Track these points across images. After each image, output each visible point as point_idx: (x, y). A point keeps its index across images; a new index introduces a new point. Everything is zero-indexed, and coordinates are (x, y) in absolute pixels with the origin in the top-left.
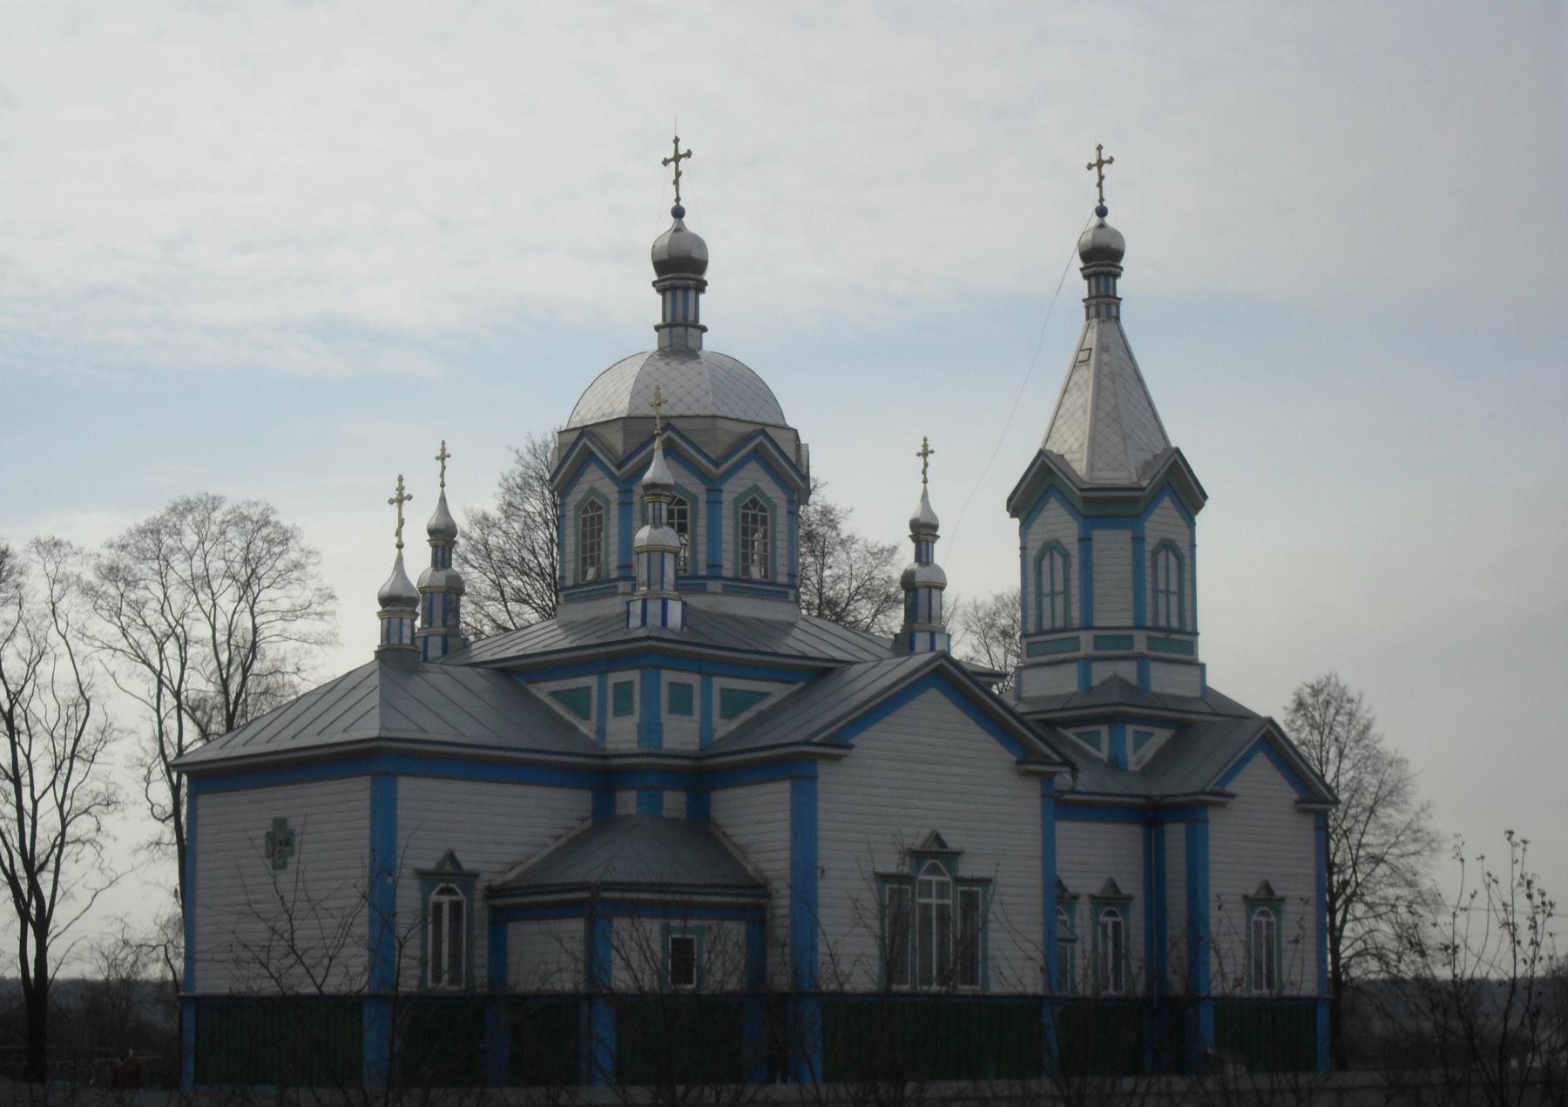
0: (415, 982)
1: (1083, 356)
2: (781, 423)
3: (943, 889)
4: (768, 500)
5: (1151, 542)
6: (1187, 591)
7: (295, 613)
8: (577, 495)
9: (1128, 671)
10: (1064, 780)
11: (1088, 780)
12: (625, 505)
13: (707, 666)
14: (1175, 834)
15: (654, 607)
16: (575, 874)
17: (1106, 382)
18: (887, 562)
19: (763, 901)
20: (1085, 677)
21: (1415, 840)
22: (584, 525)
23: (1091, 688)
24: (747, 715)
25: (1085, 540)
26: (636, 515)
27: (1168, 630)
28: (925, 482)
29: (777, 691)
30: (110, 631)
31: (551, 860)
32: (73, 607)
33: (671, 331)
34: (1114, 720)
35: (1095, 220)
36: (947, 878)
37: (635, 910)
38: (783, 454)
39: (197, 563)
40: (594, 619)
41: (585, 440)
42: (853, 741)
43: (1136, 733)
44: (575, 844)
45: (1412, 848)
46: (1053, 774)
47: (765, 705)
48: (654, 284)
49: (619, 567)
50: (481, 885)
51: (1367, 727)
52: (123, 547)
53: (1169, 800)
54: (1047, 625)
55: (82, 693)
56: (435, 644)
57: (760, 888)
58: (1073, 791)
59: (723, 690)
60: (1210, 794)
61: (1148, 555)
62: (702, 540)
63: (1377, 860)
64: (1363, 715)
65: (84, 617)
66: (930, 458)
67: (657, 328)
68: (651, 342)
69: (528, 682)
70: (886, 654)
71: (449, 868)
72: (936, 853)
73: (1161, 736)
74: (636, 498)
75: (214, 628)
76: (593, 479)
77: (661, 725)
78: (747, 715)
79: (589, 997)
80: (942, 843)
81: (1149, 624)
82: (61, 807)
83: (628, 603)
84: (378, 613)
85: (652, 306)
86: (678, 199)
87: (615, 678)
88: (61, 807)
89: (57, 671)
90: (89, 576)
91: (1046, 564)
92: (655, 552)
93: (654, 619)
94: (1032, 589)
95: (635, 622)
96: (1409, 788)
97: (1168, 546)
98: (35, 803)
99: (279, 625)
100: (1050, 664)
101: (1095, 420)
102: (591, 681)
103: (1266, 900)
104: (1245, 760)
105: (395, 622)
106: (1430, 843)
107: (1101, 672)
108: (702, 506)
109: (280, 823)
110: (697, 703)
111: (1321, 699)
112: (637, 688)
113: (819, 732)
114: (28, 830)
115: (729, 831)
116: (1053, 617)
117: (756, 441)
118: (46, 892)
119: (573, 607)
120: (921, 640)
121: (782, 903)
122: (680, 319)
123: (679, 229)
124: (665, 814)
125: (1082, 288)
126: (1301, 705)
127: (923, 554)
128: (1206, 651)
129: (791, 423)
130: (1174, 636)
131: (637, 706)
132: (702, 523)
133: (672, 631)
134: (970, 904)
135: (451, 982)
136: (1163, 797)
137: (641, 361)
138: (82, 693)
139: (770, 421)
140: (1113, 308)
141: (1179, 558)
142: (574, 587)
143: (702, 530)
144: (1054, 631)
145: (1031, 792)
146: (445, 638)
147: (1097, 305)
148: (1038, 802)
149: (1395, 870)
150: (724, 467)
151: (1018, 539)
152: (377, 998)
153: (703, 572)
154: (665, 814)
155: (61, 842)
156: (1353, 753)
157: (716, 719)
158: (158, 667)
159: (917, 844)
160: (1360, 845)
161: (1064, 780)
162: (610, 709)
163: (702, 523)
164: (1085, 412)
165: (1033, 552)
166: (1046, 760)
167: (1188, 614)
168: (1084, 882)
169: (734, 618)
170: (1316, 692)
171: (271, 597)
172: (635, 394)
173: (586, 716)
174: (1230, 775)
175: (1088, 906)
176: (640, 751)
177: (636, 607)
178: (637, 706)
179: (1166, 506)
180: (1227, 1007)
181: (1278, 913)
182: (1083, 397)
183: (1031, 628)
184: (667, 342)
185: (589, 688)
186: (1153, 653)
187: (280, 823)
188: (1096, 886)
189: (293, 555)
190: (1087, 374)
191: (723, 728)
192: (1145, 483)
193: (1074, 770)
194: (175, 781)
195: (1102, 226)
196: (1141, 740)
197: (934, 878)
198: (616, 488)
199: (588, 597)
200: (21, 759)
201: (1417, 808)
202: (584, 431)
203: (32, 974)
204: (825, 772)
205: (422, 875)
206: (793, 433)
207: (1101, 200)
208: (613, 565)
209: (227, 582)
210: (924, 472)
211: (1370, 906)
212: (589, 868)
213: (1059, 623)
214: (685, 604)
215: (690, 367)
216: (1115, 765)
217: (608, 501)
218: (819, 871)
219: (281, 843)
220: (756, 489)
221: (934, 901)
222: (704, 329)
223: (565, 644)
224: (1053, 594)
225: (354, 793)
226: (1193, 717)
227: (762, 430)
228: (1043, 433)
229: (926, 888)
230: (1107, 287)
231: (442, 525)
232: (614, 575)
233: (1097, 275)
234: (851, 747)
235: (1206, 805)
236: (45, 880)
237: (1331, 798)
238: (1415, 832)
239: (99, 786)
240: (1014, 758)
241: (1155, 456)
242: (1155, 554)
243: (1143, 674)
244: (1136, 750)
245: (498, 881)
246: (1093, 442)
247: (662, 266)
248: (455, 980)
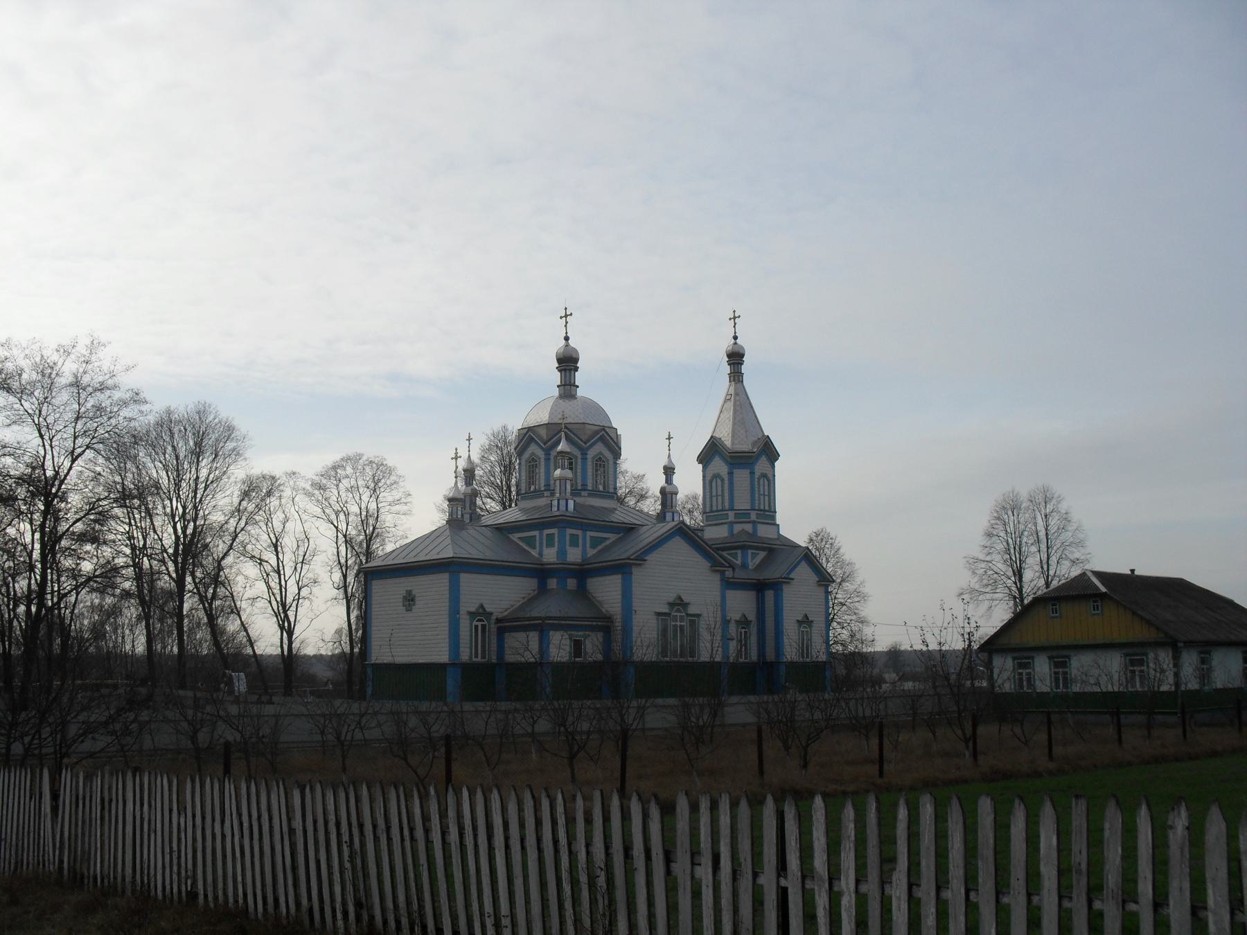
0: (467, 658)
1: (728, 397)
2: (609, 425)
3: (682, 619)
4: (606, 458)
5: (757, 475)
6: (772, 494)
7: (398, 502)
8: (526, 455)
9: (749, 528)
10: (729, 573)
11: (740, 574)
12: (547, 460)
13: (584, 527)
14: (769, 595)
15: (563, 503)
16: (535, 613)
17: (738, 408)
18: (640, 481)
19: (610, 624)
20: (731, 529)
21: (857, 596)
22: (530, 468)
23: (733, 535)
24: (600, 547)
25: (730, 474)
26: (552, 464)
27: (765, 511)
28: (669, 450)
29: (612, 537)
30: (318, 511)
31: (522, 607)
32: (301, 500)
33: (564, 388)
34: (744, 548)
35: (733, 341)
36: (684, 614)
37: (556, 628)
38: (612, 438)
39: (353, 482)
40: (535, 507)
42: (646, 558)
43: (752, 553)
44: (530, 601)
45: (856, 599)
46: (725, 571)
47: (608, 542)
48: (557, 368)
49: (545, 486)
50: (494, 617)
51: (839, 549)
52: (322, 475)
53: (767, 581)
54: (714, 508)
55: (306, 537)
56: (467, 517)
57: (609, 619)
58: (732, 578)
59: (591, 536)
60: (784, 578)
61: (756, 480)
62: (579, 474)
63: (843, 604)
64: (836, 545)
65: (305, 504)
66: (671, 440)
67: (558, 386)
68: (556, 392)
69: (509, 533)
70: (655, 521)
71: (481, 611)
72: (679, 604)
73: (762, 554)
74: (552, 457)
75: (360, 509)
76: (533, 448)
77: (566, 551)
78: (600, 547)
79: (541, 664)
80: (682, 600)
81: (757, 508)
82: (298, 584)
83: (551, 501)
85: (556, 377)
86: (566, 333)
87: (547, 532)
88: (298, 584)
89: (294, 527)
90: (308, 487)
91: (714, 484)
92: (563, 480)
93: (563, 508)
94: (708, 494)
95: (555, 509)
96: (855, 575)
97: (764, 476)
98: (286, 582)
99: (388, 507)
100: (716, 525)
101: (734, 424)
102: (536, 533)
103: (805, 621)
104: (796, 566)
105: (455, 508)
106: (863, 598)
107: (737, 528)
108: (579, 460)
109: (409, 593)
110: (580, 541)
111: (819, 538)
112: (556, 536)
113: (632, 555)
114: (284, 594)
116: (717, 505)
117: (601, 434)
118: (292, 619)
119: (524, 502)
120: (669, 516)
121: (618, 624)
122: (568, 383)
123: (567, 345)
124: (568, 588)
125: (727, 369)
126: (811, 540)
127: (669, 480)
128: (779, 519)
129: (614, 426)
130: (767, 513)
131: (556, 544)
132: (579, 467)
133: (570, 512)
134: (692, 623)
135: (745, 659)
136: (764, 579)
137: (552, 401)
138: (306, 537)
139: (606, 425)
140: (741, 377)
141: (769, 481)
142: (525, 493)
143: (579, 471)
144: (718, 511)
145: (716, 578)
146: (471, 515)
147: (734, 376)
148: (719, 583)
149: (848, 607)
150: (588, 444)
151: (702, 473)
152: (453, 665)
154: (568, 588)
155: (298, 598)
156: (832, 561)
157: (588, 549)
158: (336, 525)
159: (671, 600)
160: (835, 598)
161: (729, 573)
162: (545, 544)
163: (579, 467)
164: (730, 420)
165: (708, 478)
166: (723, 565)
167: (772, 504)
168: (735, 615)
169: (592, 506)
170: (817, 536)
171: (386, 496)
172: (551, 414)
174: (791, 571)
175: (735, 625)
176: (558, 562)
177: (555, 503)
178: (556, 544)
179: (764, 458)
180: (792, 664)
181: (810, 627)
182: (729, 414)
183: (708, 510)
184: (563, 392)
186: (759, 520)
187: (409, 593)
188: (737, 617)
189: (393, 478)
190: (730, 405)
191: (591, 552)
192: (755, 450)
193: (734, 569)
194: (344, 572)
195: (735, 343)
196: (754, 556)
197: (678, 614)
198: (543, 453)
199: (532, 498)
200: (281, 565)
201: (859, 583)
202: (530, 429)
203: (286, 653)
204: (635, 570)
205: (470, 613)
206: (614, 431)
207: (735, 333)
208: (542, 485)
209: (366, 489)
210: (669, 446)
211: (838, 623)
212: (539, 610)
213: (720, 508)
214: (575, 501)
215: (573, 402)
216: (744, 566)
217: (540, 458)
218: (634, 612)
219: (409, 600)
220: (601, 453)
221: (678, 623)
222: (578, 387)
225: (443, 579)
226: (775, 546)
227: (603, 428)
228: (712, 429)
229: (675, 619)
230: (738, 369)
231: (469, 468)
232: (543, 489)
233: (733, 364)
234: (645, 560)
235: (631, 565)
236: (291, 614)
237: (831, 580)
238: (858, 593)
239: (310, 575)
240: (710, 565)
241: (759, 439)
242: (759, 479)
243: (755, 530)
244: (752, 560)
245: (500, 616)
246: (733, 431)
247: (560, 360)
248: (483, 657)
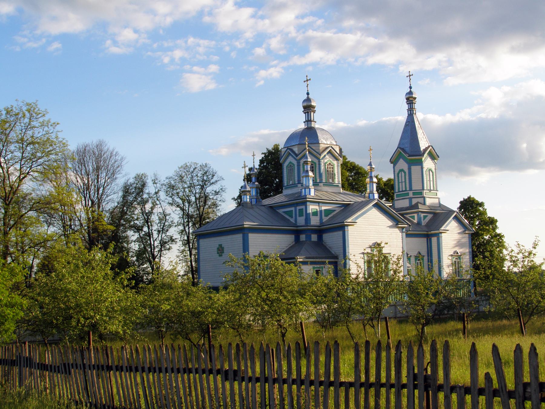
24: (330, 216)
25: (410, 169)
41: (288, 150)
54: (401, 190)
78: (330, 216)
84: (496, 221)
87: (298, 208)
91: (400, 174)
102: (293, 209)
109: (220, 246)
115: (327, 244)
119: (297, 191)
140: (409, 113)
144: (403, 191)
153: (297, 183)
173: (292, 217)
185: (292, 211)
187: (220, 246)
188: (415, 253)
198: (296, 162)
213: (404, 189)
219: (221, 250)
223: (286, 200)
224: (402, 182)
